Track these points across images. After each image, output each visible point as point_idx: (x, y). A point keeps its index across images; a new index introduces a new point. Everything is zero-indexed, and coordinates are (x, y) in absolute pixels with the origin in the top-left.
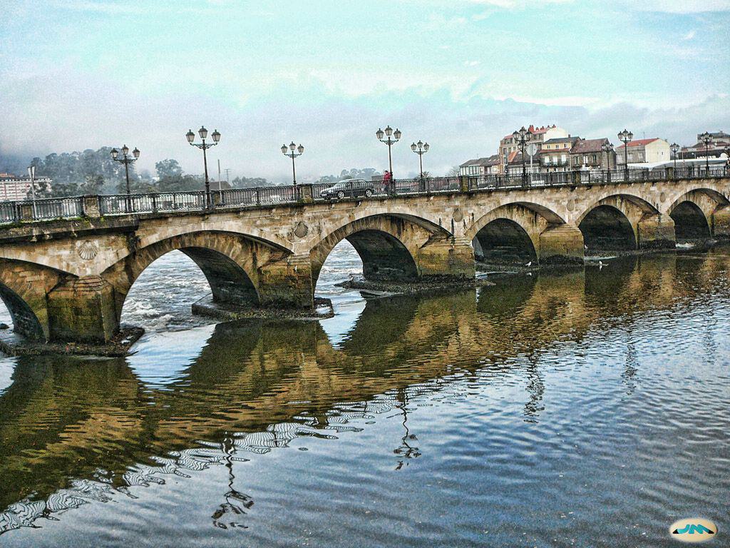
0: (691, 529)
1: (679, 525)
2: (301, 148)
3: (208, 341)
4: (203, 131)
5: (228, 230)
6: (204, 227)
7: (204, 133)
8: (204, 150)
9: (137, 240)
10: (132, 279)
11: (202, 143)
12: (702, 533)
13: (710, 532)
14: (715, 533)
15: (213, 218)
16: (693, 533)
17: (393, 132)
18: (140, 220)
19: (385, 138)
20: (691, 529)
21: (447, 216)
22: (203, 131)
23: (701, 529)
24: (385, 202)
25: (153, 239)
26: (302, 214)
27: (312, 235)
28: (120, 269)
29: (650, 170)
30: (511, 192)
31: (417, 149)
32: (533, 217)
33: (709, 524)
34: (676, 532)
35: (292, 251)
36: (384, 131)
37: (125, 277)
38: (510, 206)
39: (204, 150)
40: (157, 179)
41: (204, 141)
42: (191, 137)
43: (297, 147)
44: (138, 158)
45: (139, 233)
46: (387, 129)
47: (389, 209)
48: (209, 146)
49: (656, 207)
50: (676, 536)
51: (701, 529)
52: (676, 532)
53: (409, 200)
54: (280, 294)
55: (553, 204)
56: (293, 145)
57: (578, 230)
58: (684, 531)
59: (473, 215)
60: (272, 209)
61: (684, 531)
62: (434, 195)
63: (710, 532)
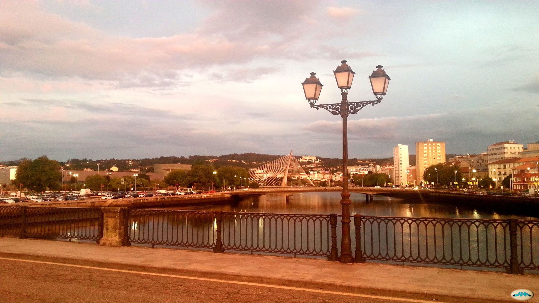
0: (521, 294)
1: (515, 292)
11: (339, 100)
12: (526, 296)
13: (530, 296)
16: (522, 296)
20: (521, 294)
23: (525, 294)
29: (459, 168)
34: (514, 296)
48: (356, 107)
50: (514, 297)
51: (525, 294)
52: (514, 296)
53: (436, 294)
54: (433, 205)
58: (518, 295)
60: (33, 237)
61: (518, 295)
63: (530, 296)
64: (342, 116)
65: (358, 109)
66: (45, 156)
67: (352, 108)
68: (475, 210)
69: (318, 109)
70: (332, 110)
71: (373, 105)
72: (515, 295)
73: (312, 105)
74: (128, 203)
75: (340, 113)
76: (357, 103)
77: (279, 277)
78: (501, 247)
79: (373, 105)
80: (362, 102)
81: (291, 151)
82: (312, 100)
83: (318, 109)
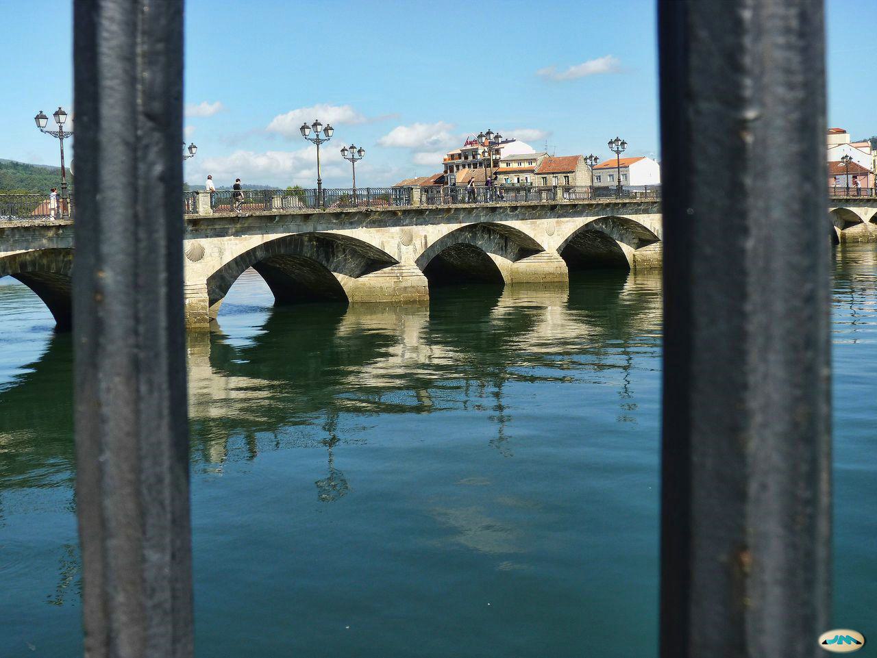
0: (839, 640)
3: (41, 358)
11: (58, 130)
13: (858, 643)
14: (863, 644)
16: (842, 643)
21: (393, 238)
23: (849, 640)
27: (209, 258)
32: (503, 242)
33: (858, 637)
34: (825, 643)
39: (61, 139)
46: (57, 114)
49: (656, 234)
50: (825, 646)
51: (849, 640)
55: (529, 226)
57: (561, 259)
58: (833, 641)
61: (833, 641)
63: (858, 643)
72: (827, 642)
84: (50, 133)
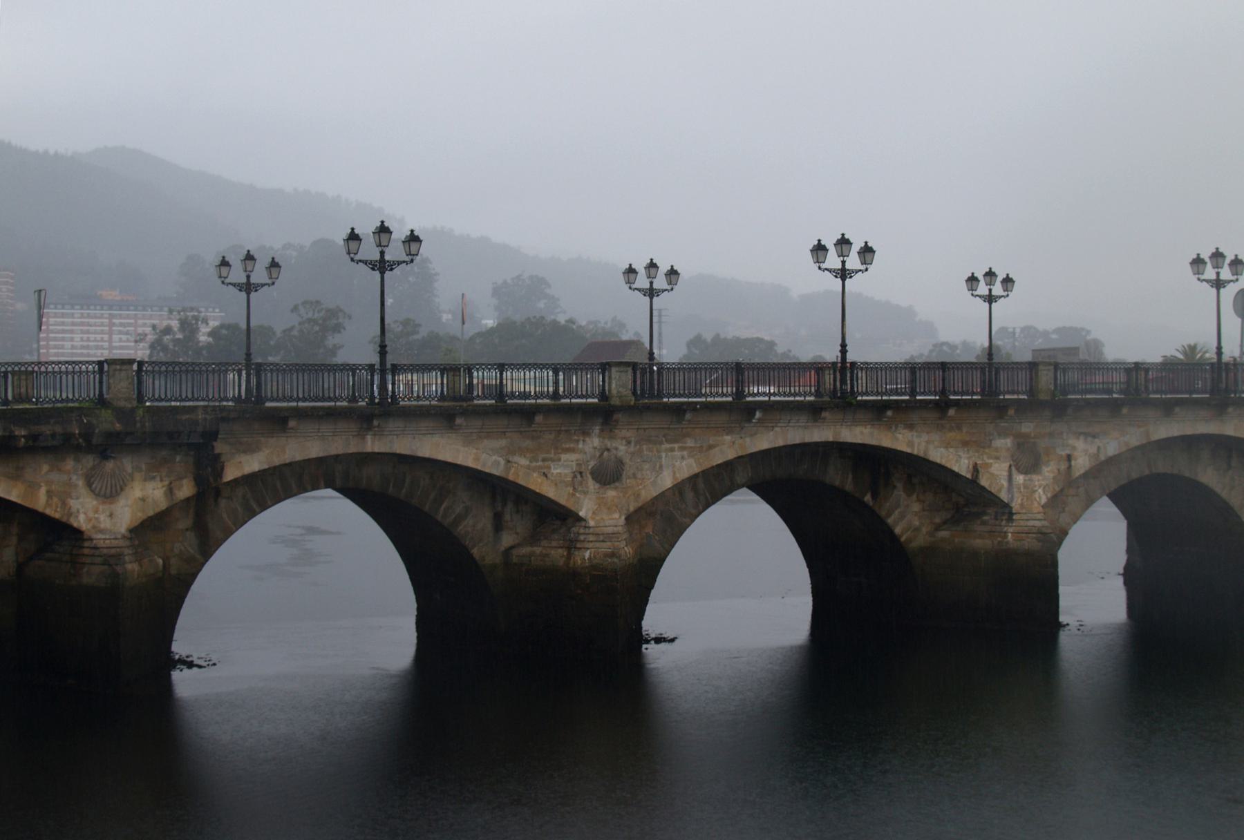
2: (1008, 281)
4: (843, 242)
5: (427, 455)
6: (372, 445)
7: (845, 247)
8: (382, 273)
9: (217, 465)
10: (207, 547)
11: (840, 267)
15: (393, 425)
17: (1228, 261)
18: (223, 419)
19: (1210, 273)
22: (843, 242)
24: (824, 414)
25: (253, 464)
26: (611, 431)
28: (184, 522)
30: (1177, 409)
31: (237, 275)
35: (582, 514)
36: (1207, 260)
37: (187, 544)
38: (1190, 443)
39: (382, 273)
40: (490, 323)
41: (990, 290)
42: (868, 256)
43: (1000, 279)
44: (676, 288)
45: (219, 447)
47: (477, 459)
48: (392, 265)
56: (652, 265)
59: (1069, 458)
60: (534, 414)
62: (957, 403)
64: (380, 273)
65: (394, 267)
66: (718, 335)
67: (388, 266)
68: (213, 343)
69: (357, 263)
70: (371, 266)
71: (407, 264)
73: (223, 282)
74: (164, 489)
75: (378, 269)
76: (393, 261)
77: (466, 449)
78: (813, 380)
79: (407, 264)
80: (398, 262)
81: (463, 294)
82: (223, 280)
83: (357, 263)
84: (365, 262)
